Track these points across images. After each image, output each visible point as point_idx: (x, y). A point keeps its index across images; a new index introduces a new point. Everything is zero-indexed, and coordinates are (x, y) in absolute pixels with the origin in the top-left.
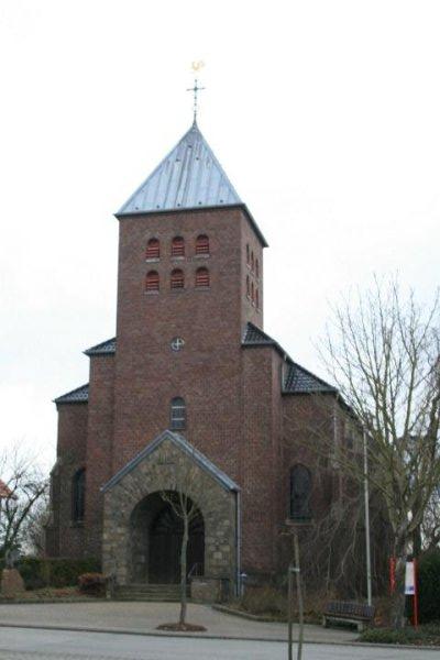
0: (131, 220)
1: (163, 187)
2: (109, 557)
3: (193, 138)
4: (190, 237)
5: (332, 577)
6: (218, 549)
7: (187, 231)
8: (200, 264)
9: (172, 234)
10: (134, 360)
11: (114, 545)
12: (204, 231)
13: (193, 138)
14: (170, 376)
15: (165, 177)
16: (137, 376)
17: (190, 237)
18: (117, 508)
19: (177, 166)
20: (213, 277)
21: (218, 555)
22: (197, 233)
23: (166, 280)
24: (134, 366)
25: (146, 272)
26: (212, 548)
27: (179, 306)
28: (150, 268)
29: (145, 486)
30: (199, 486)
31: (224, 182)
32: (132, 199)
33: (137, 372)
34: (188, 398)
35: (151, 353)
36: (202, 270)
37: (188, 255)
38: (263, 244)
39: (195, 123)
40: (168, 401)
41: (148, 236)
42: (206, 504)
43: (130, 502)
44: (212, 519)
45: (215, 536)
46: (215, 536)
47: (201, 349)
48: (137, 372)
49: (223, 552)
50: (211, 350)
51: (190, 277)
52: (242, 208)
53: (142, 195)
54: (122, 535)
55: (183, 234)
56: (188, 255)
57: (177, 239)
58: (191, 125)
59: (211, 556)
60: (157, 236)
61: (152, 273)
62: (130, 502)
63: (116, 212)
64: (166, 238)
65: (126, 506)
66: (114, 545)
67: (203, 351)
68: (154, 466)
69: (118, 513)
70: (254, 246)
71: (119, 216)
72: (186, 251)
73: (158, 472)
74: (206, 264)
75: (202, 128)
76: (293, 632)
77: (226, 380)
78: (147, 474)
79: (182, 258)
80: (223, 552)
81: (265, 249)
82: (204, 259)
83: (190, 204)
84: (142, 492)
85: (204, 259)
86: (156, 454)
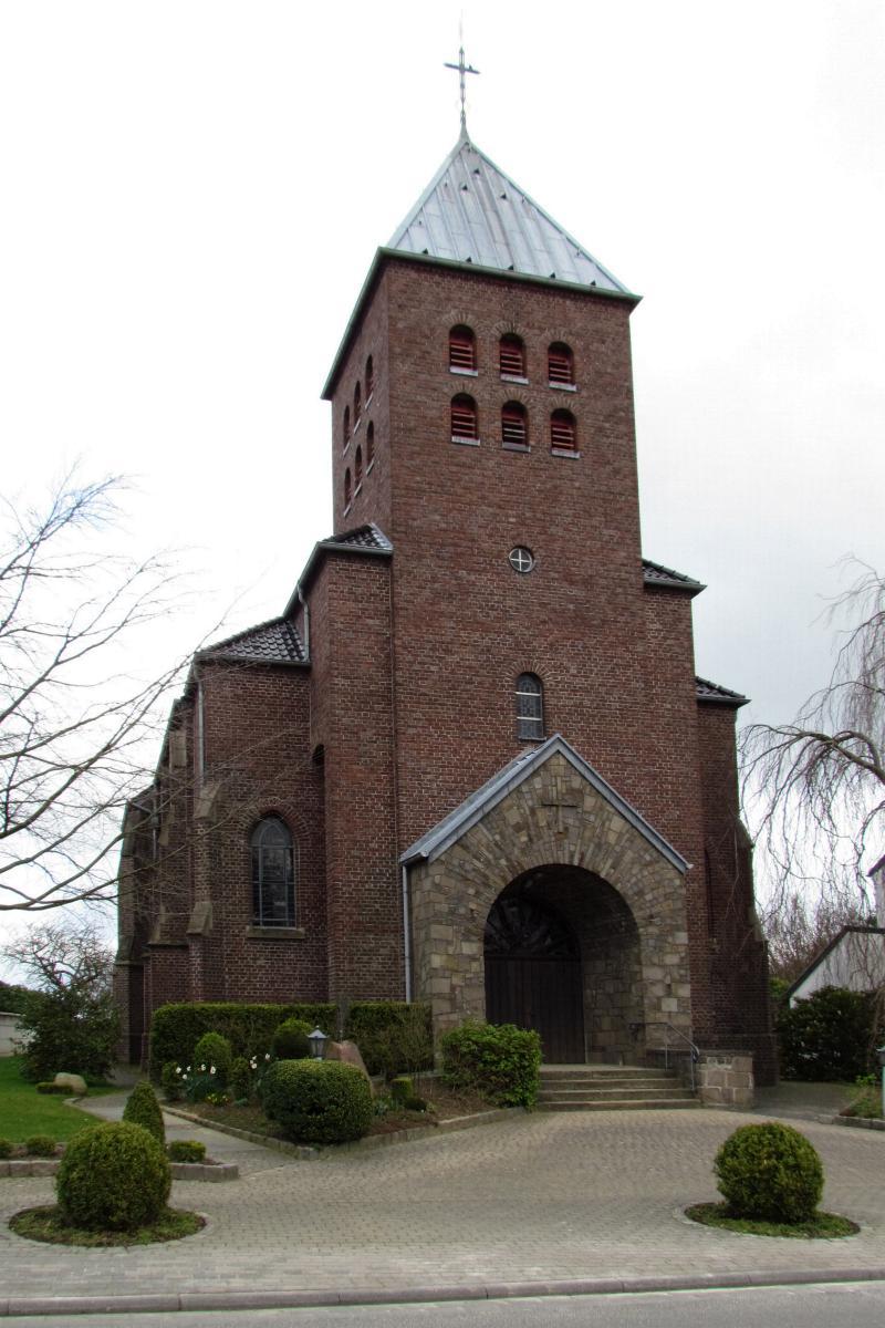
0: (414, 275)
2: (446, 1006)
3: (466, 149)
4: (537, 344)
5: (74, 1102)
6: (669, 991)
10: (434, 579)
11: (456, 980)
13: (466, 149)
14: (511, 624)
16: (442, 614)
18: (461, 898)
21: (671, 1005)
24: (437, 594)
25: (452, 394)
26: (658, 991)
27: (522, 480)
29: (516, 851)
33: (443, 606)
34: (548, 681)
35: (471, 570)
37: (483, 374)
40: (508, 678)
41: (451, 317)
42: (640, 893)
43: (486, 885)
44: (653, 930)
45: (663, 966)
46: (663, 966)
47: (569, 579)
48: (443, 606)
49: (679, 998)
50: (588, 583)
51: (539, 420)
54: (473, 958)
56: (483, 374)
59: (657, 1008)
60: (470, 321)
62: (486, 885)
64: (489, 334)
65: (478, 894)
66: (456, 980)
67: (572, 583)
68: (533, 812)
69: (462, 911)
72: (529, 368)
73: (543, 824)
75: (476, 140)
77: (620, 650)
78: (518, 828)
80: (679, 998)
82: (564, 393)
84: (511, 867)
85: (564, 393)
86: (538, 783)
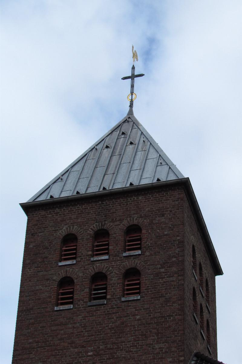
0: (43, 213)
1: (88, 172)
4: (117, 231)
7: (113, 221)
8: (128, 264)
9: (96, 226)
12: (136, 220)
15: (91, 163)
17: (117, 231)
19: (106, 153)
20: (146, 280)
22: (126, 223)
23: (82, 291)
28: (63, 274)
30: (24, 353)
31: (162, 160)
32: (48, 188)
36: (132, 274)
38: (219, 272)
39: (131, 112)
41: (63, 231)
51: (115, 280)
52: (184, 185)
53: (59, 185)
55: (108, 225)
57: (102, 234)
58: (125, 115)
60: (75, 229)
61: (66, 282)
63: (25, 200)
70: (207, 270)
71: (27, 208)
74: (137, 263)
75: (138, 115)
76: (138, 142)
79: (106, 257)
81: (217, 278)
83: (120, 184)
